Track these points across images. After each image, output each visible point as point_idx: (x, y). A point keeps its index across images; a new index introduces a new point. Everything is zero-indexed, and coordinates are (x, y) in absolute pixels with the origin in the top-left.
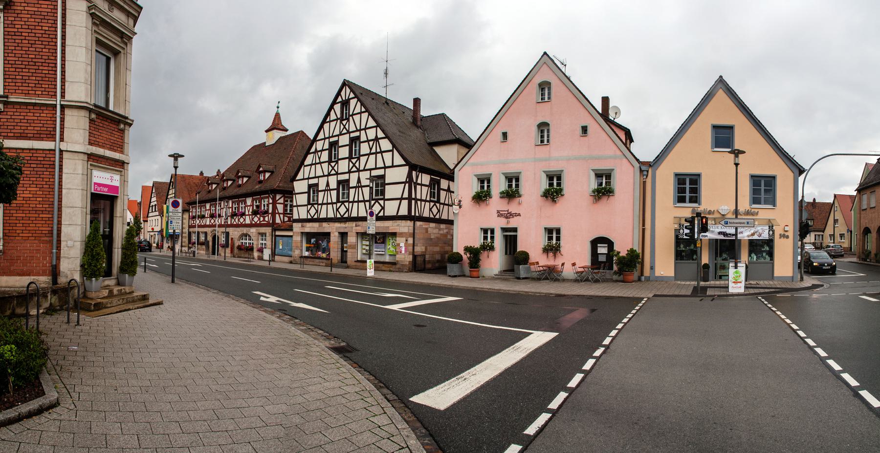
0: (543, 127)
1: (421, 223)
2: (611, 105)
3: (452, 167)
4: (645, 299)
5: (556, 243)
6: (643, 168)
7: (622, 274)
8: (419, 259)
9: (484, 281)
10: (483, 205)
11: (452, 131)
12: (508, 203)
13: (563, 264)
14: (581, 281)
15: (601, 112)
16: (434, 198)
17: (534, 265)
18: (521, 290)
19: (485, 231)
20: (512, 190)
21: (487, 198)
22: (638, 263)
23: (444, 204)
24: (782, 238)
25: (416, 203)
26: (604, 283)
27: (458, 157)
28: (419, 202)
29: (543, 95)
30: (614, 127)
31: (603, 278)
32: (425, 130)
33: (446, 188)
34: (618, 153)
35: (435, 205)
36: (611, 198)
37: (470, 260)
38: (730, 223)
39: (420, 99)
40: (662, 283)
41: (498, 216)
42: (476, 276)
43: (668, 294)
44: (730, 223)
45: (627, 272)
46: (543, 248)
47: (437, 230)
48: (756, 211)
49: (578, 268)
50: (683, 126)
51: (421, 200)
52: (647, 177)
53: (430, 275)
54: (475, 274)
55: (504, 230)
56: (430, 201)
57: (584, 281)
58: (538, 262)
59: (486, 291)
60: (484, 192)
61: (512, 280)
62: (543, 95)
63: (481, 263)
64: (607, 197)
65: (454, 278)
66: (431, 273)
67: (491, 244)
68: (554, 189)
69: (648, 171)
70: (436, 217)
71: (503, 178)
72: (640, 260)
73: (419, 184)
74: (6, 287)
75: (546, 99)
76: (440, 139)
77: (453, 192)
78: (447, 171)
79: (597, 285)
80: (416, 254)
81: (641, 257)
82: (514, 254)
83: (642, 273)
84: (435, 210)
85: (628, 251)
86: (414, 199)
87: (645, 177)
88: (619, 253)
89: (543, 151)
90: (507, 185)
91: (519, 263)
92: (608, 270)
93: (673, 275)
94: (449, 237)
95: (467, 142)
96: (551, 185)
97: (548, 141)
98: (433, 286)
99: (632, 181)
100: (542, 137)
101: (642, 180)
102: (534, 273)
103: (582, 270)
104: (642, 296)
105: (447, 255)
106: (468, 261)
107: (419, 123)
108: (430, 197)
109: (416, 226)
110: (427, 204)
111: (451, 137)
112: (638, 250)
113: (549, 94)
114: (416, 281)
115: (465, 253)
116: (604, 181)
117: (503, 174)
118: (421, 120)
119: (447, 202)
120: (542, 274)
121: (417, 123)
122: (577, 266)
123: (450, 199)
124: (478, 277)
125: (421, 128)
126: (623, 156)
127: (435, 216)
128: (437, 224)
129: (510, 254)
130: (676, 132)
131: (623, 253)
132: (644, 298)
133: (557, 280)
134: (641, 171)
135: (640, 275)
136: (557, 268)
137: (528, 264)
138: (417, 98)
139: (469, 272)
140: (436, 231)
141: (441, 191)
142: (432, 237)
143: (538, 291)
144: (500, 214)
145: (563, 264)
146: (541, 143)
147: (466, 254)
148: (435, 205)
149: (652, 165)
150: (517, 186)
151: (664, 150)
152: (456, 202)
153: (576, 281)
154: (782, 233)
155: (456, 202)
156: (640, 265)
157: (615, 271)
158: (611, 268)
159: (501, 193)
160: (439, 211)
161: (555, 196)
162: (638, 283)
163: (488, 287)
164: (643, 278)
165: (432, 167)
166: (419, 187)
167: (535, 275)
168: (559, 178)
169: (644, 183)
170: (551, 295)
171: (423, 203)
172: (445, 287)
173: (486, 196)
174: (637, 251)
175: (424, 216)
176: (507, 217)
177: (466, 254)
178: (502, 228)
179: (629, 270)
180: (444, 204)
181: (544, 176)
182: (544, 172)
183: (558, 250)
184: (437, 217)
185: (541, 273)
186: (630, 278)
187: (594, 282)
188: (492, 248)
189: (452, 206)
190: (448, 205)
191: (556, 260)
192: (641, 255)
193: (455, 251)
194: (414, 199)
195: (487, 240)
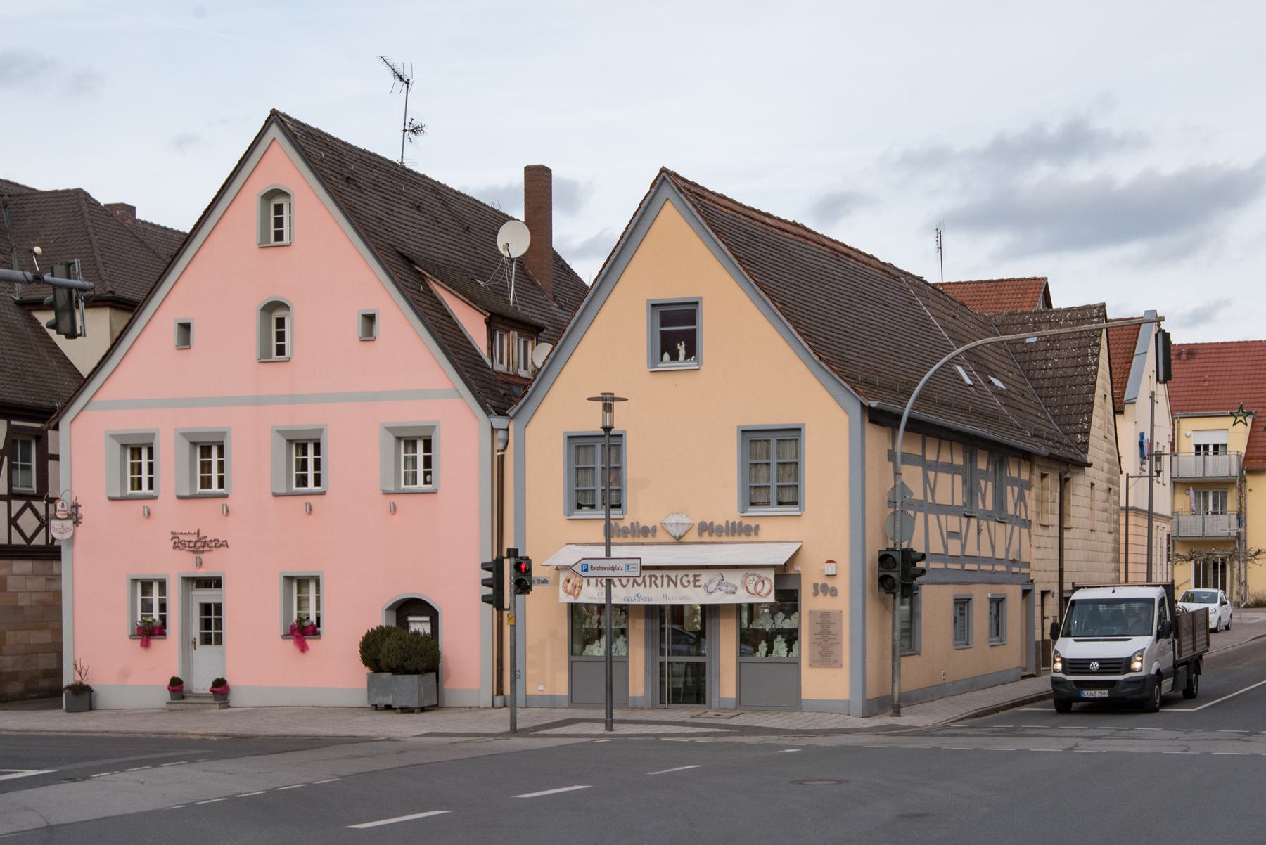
0: (275, 313)
24: (821, 594)
35: (28, 505)
38: (593, 568)
44: (593, 568)
47: (42, 580)
48: (753, 523)
70: (34, 543)
89: (276, 377)
142: (21, 603)
144: (178, 542)
154: (821, 581)
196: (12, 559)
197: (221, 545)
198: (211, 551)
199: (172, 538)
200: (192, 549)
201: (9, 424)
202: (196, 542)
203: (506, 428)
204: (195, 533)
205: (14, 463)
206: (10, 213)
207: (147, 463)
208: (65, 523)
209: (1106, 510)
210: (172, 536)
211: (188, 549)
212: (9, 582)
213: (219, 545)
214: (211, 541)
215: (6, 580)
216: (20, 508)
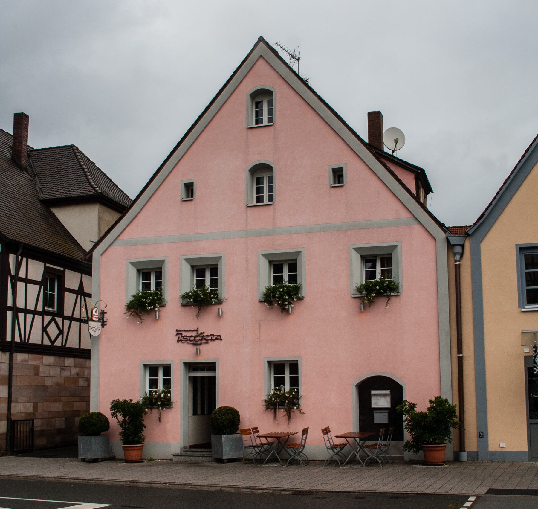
1: (25, 356)
2: (386, 125)
3: (87, 247)
4: (472, 499)
5: (290, 390)
6: (454, 240)
7: (422, 448)
8: (21, 429)
9: (153, 469)
10: (148, 320)
11: (88, 180)
12: (198, 316)
13: (305, 431)
14: (342, 463)
15: (367, 140)
16: (52, 306)
17: (250, 433)
18: (226, 484)
19: (153, 370)
20: (204, 292)
21: (155, 307)
22: (454, 425)
23: (72, 319)
25: (15, 317)
26: (387, 466)
27: (99, 229)
28: (21, 316)
29: (258, 114)
30: (393, 168)
31: (383, 457)
32: (35, 175)
33: (76, 288)
34: (404, 214)
35: (53, 320)
36: (393, 300)
37: (124, 428)
39: (27, 117)
40: (505, 465)
41: (178, 341)
42: (137, 458)
43: (517, 488)
45: (431, 443)
46: (266, 401)
49: (334, 438)
50: (499, 195)
51: (26, 311)
52: (462, 255)
53: (42, 459)
54: (134, 454)
55: (190, 367)
56: (43, 313)
57: (347, 464)
58: (257, 428)
59: (157, 488)
60: (150, 294)
61: (207, 464)
62: (258, 114)
63: (146, 433)
64: (385, 300)
65: (92, 464)
66: (44, 457)
67: (166, 396)
68: (283, 287)
69: (463, 246)
71: (187, 269)
72: (456, 420)
73: (21, 280)
74: (208, 466)
75: (265, 122)
76: (65, 193)
77: (90, 296)
78: (79, 256)
79: (373, 471)
80: (13, 418)
81: (457, 413)
82: (210, 413)
83: (461, 446)
84: (53, 330)
85: (431, 401)
86: (10, 309)
87: (458, 257)
88: (413, 406)
90: (195, 282)
91: (220, 432)
92: (393, 440)
93: (525, 447)
94: (81, 382)
95: (117, 200)
96: (278, 279)
97: (271, 198)
98: (49, 482)
99: (432, 266)
100: (259, 190)
101: (453, 264)
102: (250, 450)
103: (342, 441)
104: (464, 492)
105: (77, 420)
106: (120, 430)
107: (24, 162)
108: (45, 305)
109: (14, 362)
110: (38, 318)
111: (86, 191)
112: (452, 400)
113: (271, 112)
114: (14, 473)
115: (113, 414)
116: (379, 269)
117: (187, 260)
118: (29, 156)
119: (77, 315)
120: (266, 450)
121: (20, 161)
122: (333, 434)
123: (84, 310)
124: (142, 461)
125: (27, 172)
126: (413, 221)
127: (53, 342)
128: (57, 358)
129: (202, 413)
130: (516, 167)
131: (422, 407)
132: (468, 497)
133: (294, 462)
134: (450, 246)
135: (457, 449)
136: (294, 439)
137: (238, 432)
138: (22, 114)
139: (122, 449)
140: (56, 371)
141: (66, 294)
143: (257, 485)
145: (305, 431)
146: (257, 203)
147: (116, 417)
148: (53, 320)
149: (470, 233)
150: (214, 283)
151: (493, 204)
152: (96, 314)
153: (332, 463)
155: (96, 314)
156: (457, 430)
157: (408, 442)
158: (399, 436)
159: (184, 297)
160: (61, 332)
161: (286, 300)
162: (456, 466)
163: (161, 479)
164: (464, 456)
165: (47, 247)
166: (21, 286)
167: (252, 453)
168: (293, 267)
169: (457, 268)
170: (284, 493)
171: (29, 317)
172: (75, 484)
173: (153, 303)
174: (450, 401)
175: (30, 342)
176: (195, 343)
177: (116, 417)
178: (185, 364)
179: (434, 440)
180: (72, 319)
181: (264, 265)
182: (265, 255)
183: (294, 404)
184: (58, 343)
185: (263, 450)
186: (439, 455)
187: (367, 465)
188: (167, 403)
189: (87, 322)
190: (80, 320)
191: (292, 424)
192: (457, 409)
193: (93, 409)
194: (10, 309)
195: (157, 387)
196: (43, 355)
197: (216, 339)
198: (207, 343)
199: (177, 335)
200: (192, 342)
201: (45, 266)
202: (196, 336)
203: (462, 244)
204: (195, 330)
205: (46, 292)
206: (32, 159)
207: (154, 282)
208: (96, 324)
209: (139, 400)
210: (176, 333)
211: (188, 342)
212: (41, 370)
213: (214, 338)
214: (208, 336)
215: (39, 368)
216: (49, 321)
